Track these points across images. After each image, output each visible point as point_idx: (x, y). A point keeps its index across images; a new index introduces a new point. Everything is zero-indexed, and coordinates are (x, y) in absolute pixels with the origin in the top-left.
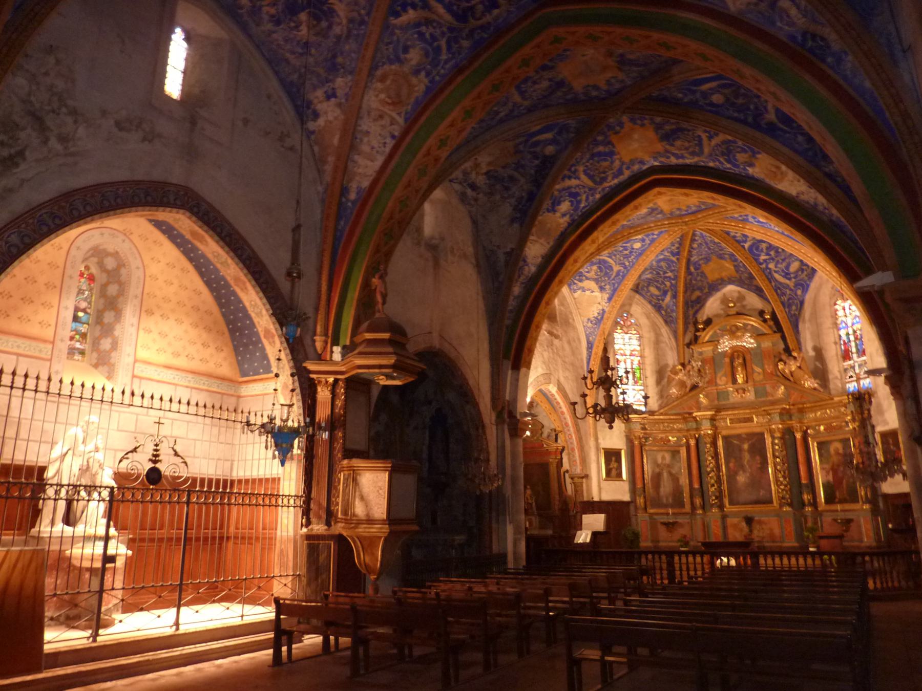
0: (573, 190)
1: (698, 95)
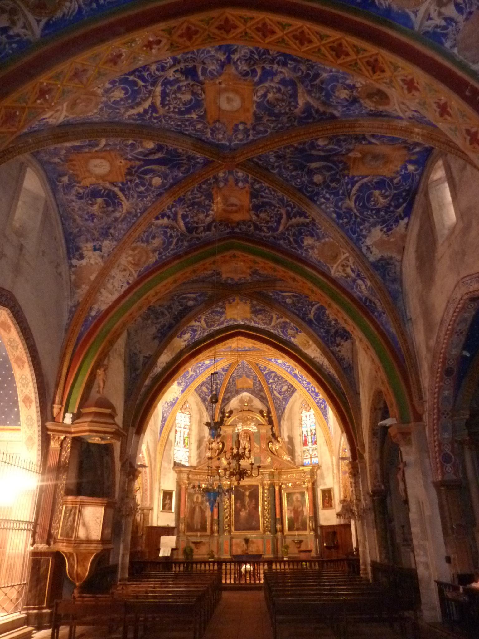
0: (195, 328)
1: (280, 297)
